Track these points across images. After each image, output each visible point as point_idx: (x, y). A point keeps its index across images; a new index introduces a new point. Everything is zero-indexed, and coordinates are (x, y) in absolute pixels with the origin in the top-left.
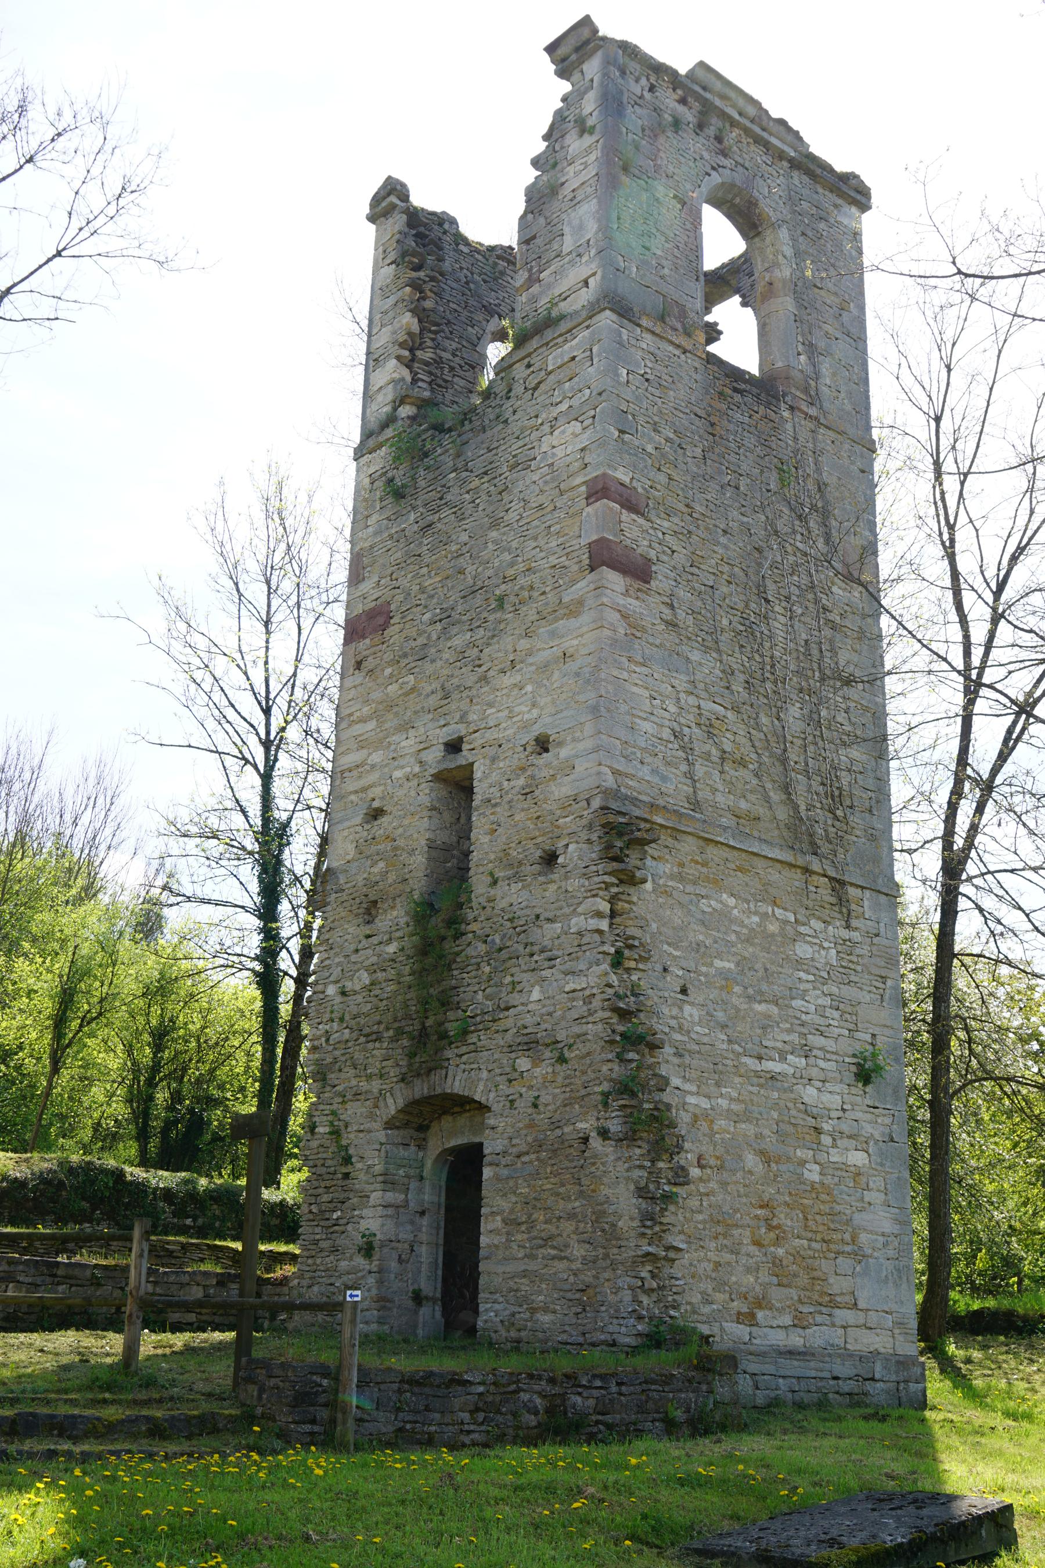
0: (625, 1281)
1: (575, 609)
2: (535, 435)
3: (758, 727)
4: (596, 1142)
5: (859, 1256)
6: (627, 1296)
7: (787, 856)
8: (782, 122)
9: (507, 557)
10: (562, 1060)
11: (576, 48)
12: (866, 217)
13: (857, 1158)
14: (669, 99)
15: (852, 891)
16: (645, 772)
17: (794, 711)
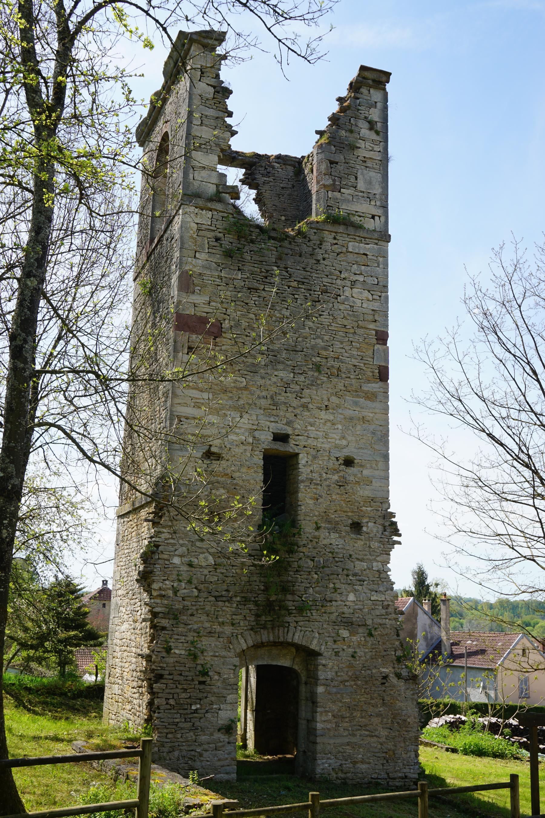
2: (339, 282)
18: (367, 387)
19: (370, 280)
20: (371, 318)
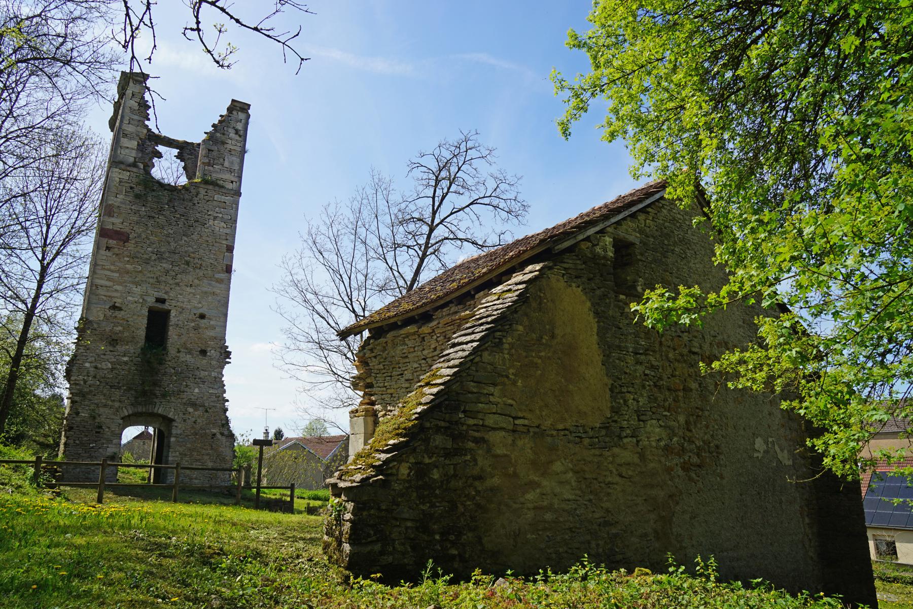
10: (207, 411)
18: (217, 276)
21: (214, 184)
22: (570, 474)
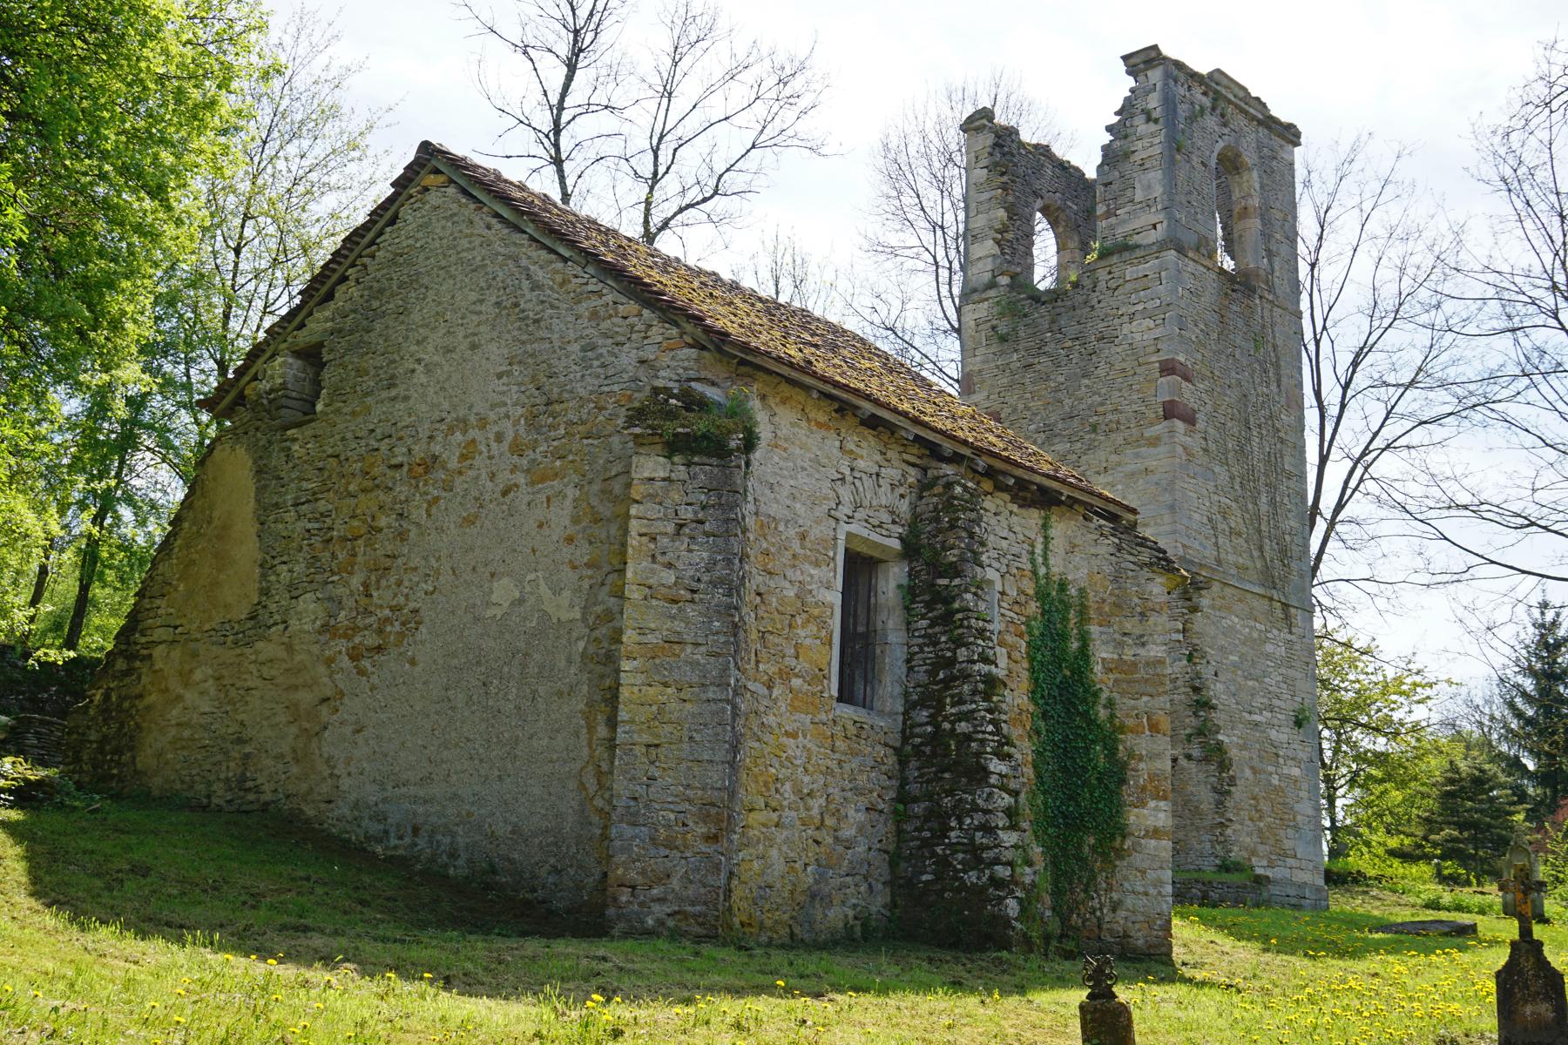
0: (1207, 837)
1: (1154, 442)
2: (1116, 321)
3: (1247, 511)
4: (1183, 762)
5: (1296, 828)
6: (1208, 845)
7: (1260, 590)
8: (1258, 99)
9: (1097, 399)
11: (1143, 62)
12: (1297, 150)
13: (1296, 772)
14: (1197, 92)
15: (1293, 610)
16: (1196, 545)
17: (1264, 499)
18: (1149, 433)
19: (1150, 305)
20: (1153, 348)
21: (1125, 248)
22: (211, 682)
